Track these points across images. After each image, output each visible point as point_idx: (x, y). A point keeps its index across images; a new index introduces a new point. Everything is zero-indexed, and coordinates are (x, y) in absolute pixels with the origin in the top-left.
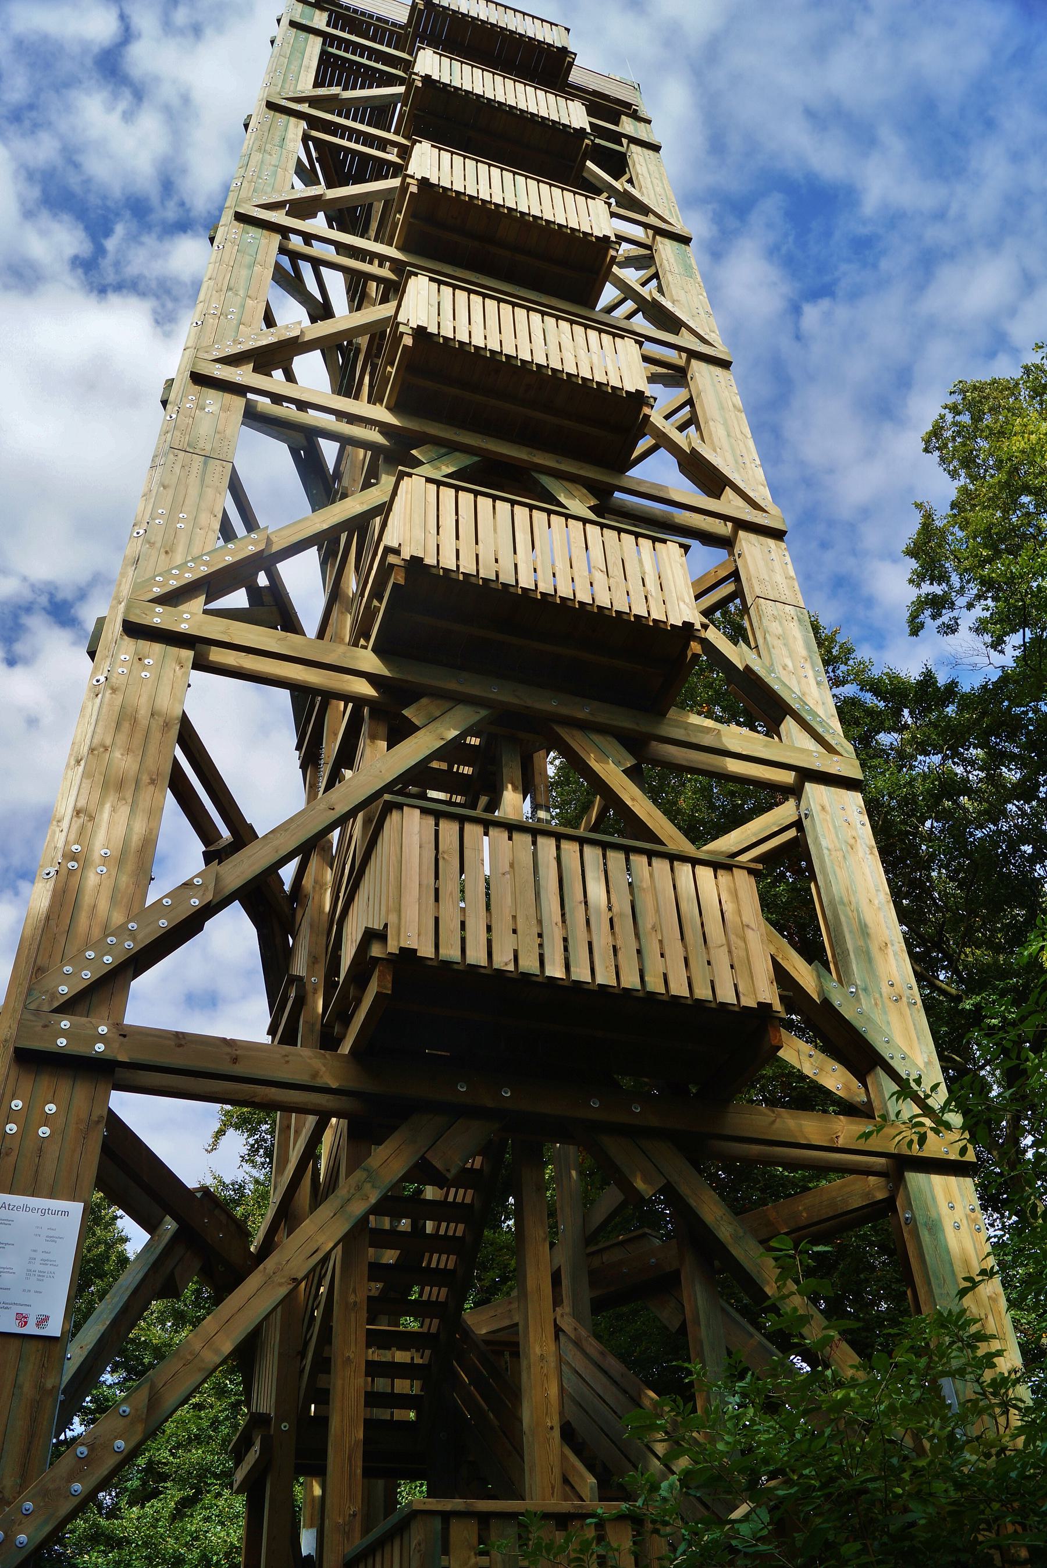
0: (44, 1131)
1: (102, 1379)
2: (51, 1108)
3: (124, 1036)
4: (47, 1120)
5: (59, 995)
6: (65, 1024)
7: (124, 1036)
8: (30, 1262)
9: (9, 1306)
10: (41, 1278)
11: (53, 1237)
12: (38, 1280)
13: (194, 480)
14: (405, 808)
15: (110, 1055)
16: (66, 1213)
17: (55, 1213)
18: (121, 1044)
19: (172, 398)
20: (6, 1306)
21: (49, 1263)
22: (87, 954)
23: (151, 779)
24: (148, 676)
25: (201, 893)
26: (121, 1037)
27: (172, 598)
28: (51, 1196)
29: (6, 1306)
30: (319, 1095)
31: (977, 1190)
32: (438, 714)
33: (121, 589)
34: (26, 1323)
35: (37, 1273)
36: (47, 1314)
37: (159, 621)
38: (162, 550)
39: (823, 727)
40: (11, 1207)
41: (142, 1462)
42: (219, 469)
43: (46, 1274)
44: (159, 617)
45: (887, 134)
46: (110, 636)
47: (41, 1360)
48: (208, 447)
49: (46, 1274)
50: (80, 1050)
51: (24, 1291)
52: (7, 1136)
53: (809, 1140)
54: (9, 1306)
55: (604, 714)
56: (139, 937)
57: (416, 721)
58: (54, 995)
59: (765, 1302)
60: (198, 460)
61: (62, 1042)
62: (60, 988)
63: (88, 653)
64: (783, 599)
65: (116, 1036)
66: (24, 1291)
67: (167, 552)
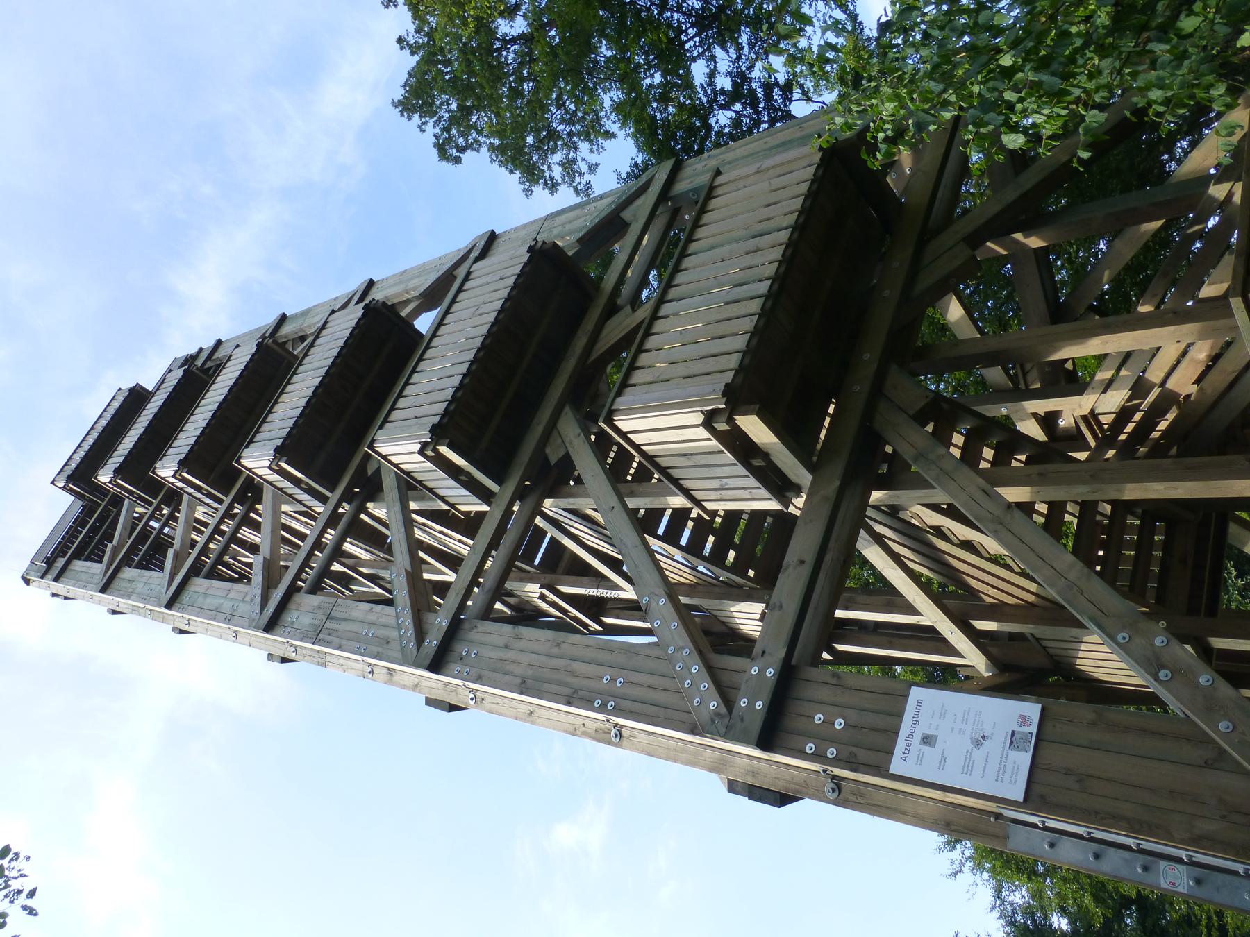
0: (839, 724)
2: (818, 718)
3: (764, 652)
4: (829, 722)
5: (717, 709)
6: (743, 702)
7: (764, 652)
8: (964, 734)
10: (980, 722)
13: (342, 626)
14: (614, 407)
15: (778, 664)
16: (919, 702)
17: (918, 711)
18: (770, 654)
19: (280, 653)
22: (686, 686)
23: (556, 646)
24: (475, 652)
25: (656, 598)
26: (765, 655)
27: (420, 635)
28: (900, 715)
32: (559, 441)
33: (408, 685)
37: (435, 642)
38: (385, 646)
39: (633, 188)
40: (907, 752)
41: (1196, 82)
42: (339, 609)
44: (432, 643)
46: (441, 692)
48: (320, 617)
50: (767, 691)
52: (839, 757)
53: (966, 538)
55: (589, 324)
56: (681, 644)
57: (561, 453)
58: (717, 714)
60: (329, 625)
61: (759, 705)
62: (712, 708)
63: (449, 711)
64: (538, 229)
65: (763, 659)
67: (388, 643)
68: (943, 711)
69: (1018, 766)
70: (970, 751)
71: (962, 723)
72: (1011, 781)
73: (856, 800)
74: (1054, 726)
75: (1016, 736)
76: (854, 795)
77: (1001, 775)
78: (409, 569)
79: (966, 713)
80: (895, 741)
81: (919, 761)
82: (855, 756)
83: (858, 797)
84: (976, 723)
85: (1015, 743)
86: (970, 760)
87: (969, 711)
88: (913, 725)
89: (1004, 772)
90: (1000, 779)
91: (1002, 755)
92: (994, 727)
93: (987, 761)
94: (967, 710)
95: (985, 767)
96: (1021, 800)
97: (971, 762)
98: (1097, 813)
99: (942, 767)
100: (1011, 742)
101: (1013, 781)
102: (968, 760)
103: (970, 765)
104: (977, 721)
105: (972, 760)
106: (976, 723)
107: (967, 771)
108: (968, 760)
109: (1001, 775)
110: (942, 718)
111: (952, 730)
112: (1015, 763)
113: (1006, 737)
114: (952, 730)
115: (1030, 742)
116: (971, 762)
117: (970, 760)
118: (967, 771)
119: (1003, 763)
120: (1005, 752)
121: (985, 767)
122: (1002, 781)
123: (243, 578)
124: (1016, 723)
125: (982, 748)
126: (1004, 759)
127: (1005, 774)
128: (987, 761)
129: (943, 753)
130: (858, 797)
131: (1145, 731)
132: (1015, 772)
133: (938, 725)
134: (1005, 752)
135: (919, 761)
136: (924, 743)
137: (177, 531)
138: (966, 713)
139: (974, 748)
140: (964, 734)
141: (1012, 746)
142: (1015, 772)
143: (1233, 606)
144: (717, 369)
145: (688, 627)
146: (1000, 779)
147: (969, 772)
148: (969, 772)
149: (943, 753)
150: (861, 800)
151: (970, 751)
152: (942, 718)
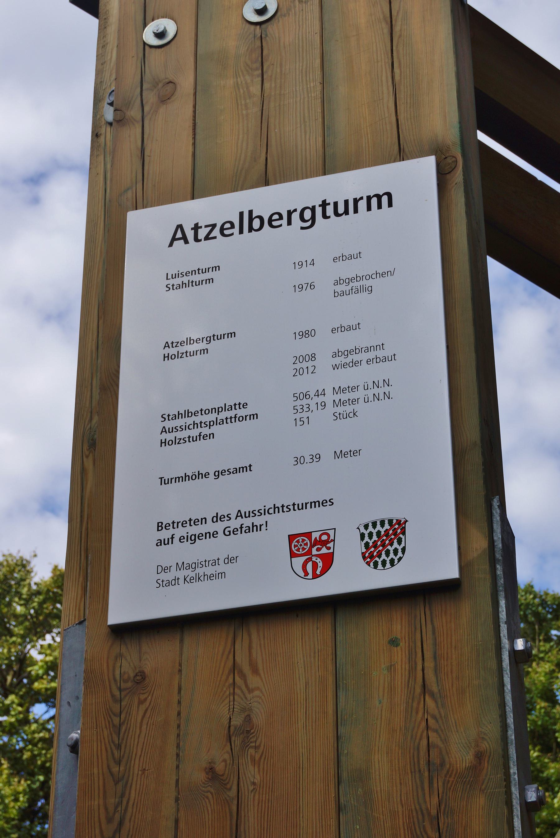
1: (27, 797)
8: (298, 372)
9: (258, 521)
10: (349, 408)
11: (357, 278)
12: (338, 417)
20: (247, 522)
21: (364, 356)
24: (170, 27)
29: (247, 522)
30: (469, 314)
31: (241, 679)
34: (328, 560)
35: (329, 398)
36: (396, 515)
43: (360, 394)
45: (32, 721)
47: (412, 670)
49: (360, 394)
51: (298, 461)
54: (258, 521)
59: (506, 598)
66: (298, 461)
77: (180, 532)
78: (62, 566)
79: (371, 355)
81: (178, 281)
82: (164, 100)
86: (210, 425)
89: (194, 539)
90: (165, 534)
91: (252, 514)
93: (218, 474)
94: (387, 352)
95: (199, 475)
97: (206, 431)
98: (119, 747)
101: (164, 576)
103: (194, 433)
108: (212, 417)
109: (180, 532)
111: (306, 334)
112: (230, 560)
114: (306, 334)
116: (206, 431)
117: (210, 425)
119: (219, 526)
121: (199, 475)
122: (160, 543)
124: (368, 519)
126: (235, 524)
128: (218, 474)
133: (312, 286)
135: (178, 281)
138: (371, 355)
143: (555, 607)
144: (197, 153)
146: (165, 534)
151: (241, 412)
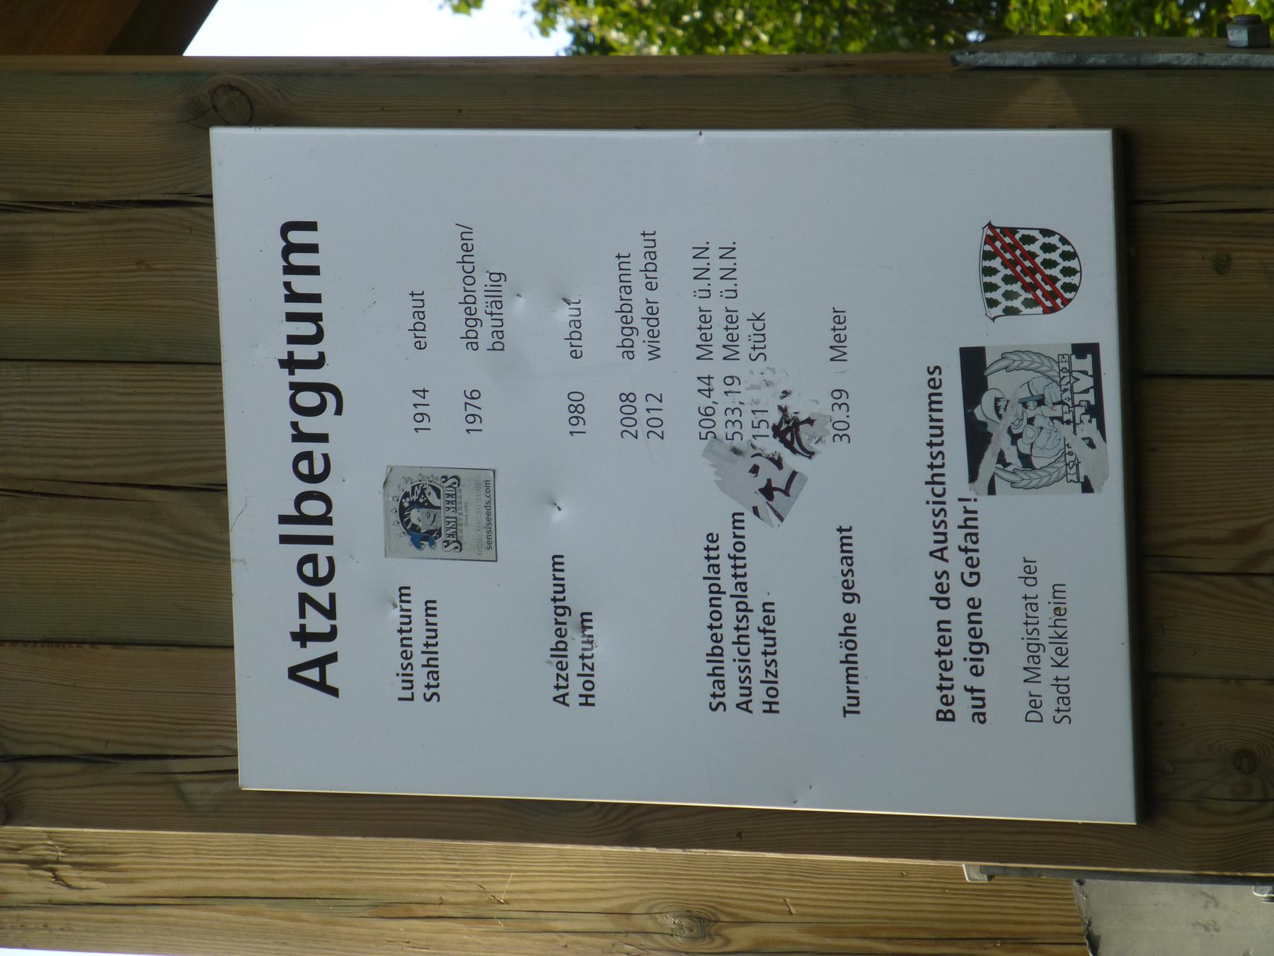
8: (656, 430)
68: (482, 280)
69: (1057, 590)
70: (726, 545)
71: (629, 353)
72: (1035, 704)
73: (62, 893)
74: (1222, 265)
75: (1000, 383)
76: (36, 864)
77: (961, 675)
79: (638, 280)
80: (220, 554)
81: (420, 677)
83: (66, 872)
84: (719, 337)
85: (1001, 441)
87: (651, 254)
88: (309, 426)
89: (978, 646)
90: (963, 704)
92: (839, 350)
93: (850, 595)
96: (1121, 810)
97: (756, 619)
99: (576, 686)
100: (978, 438)
102: (728, 606)
103: (757, 642)
104: (719, 320)
105: (754, 602)
106: (719, 337)
107: (747, 692)
108: (728, 606)
109: (961, 675)
110: (641, 349)
111: (576, 410)
112: (1030, 574)
113: (934, 403)
115: (1096, 411)
116: (756, 619)
118: (747, 692)
119: (958, 595)
120: (955, 516)
123: (767, 676)
125: (802, 506)
126: (956, 563)
127: (988, 661)
128: (850, 595)
129: (559, 584)
130: (66, 872)
131: (136, 74)
132: (1045, 634)
134: (955, 516)
135: (420, 677)
136: (421, 538)
137: (1003, 421)
138: (638, 280)
139: (749, 516)
140: (656, 430)
141: (988, 464)
142: (1045, 634)
145: (270, 74)
146: (963, 704)
147: (759, 692)
148: (759, 692)
149: (559, 584)
150: (101, 891)
151: (726, 545)
152: (641, 349)
